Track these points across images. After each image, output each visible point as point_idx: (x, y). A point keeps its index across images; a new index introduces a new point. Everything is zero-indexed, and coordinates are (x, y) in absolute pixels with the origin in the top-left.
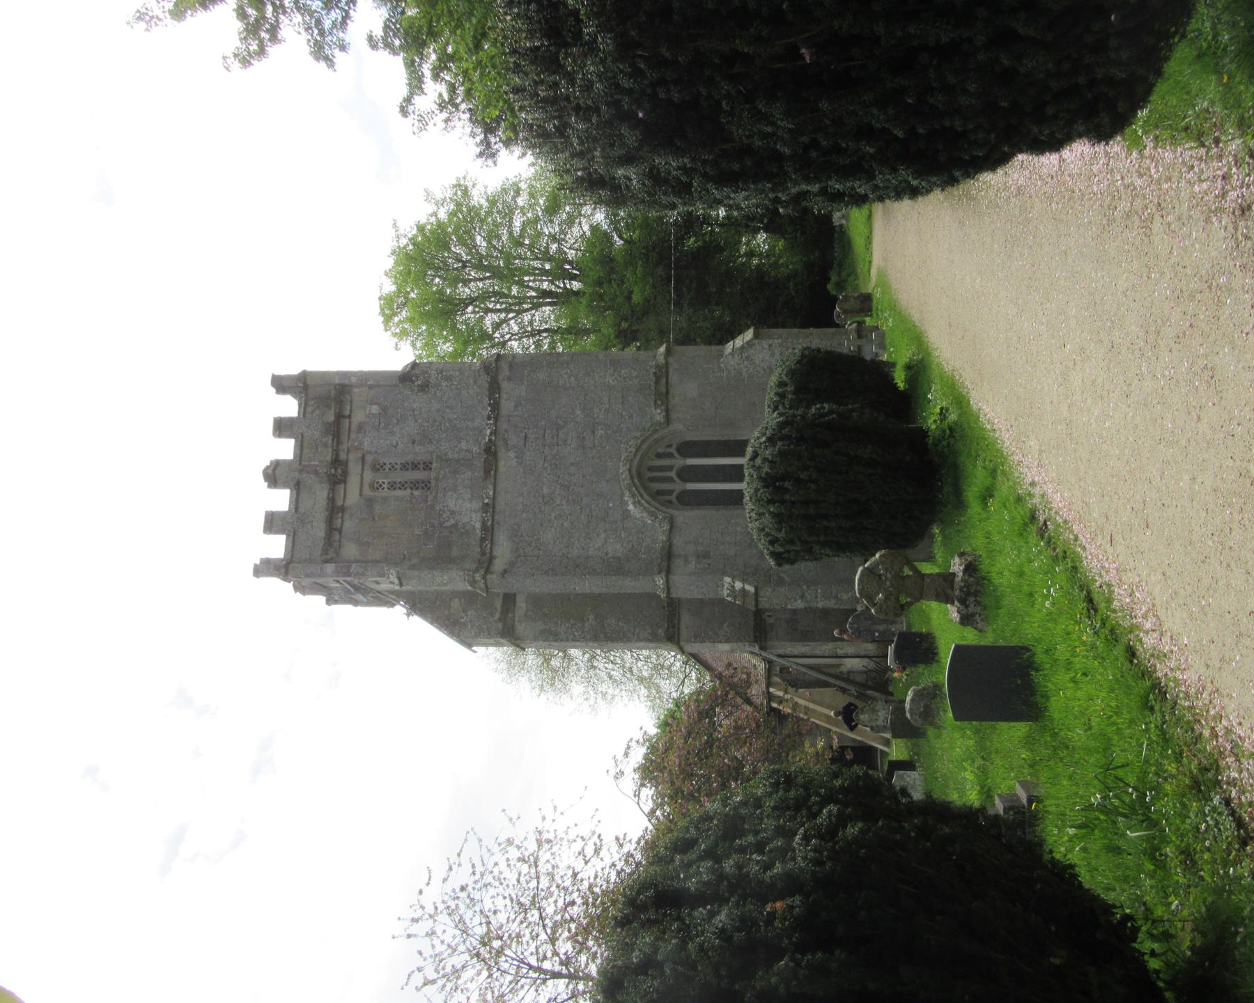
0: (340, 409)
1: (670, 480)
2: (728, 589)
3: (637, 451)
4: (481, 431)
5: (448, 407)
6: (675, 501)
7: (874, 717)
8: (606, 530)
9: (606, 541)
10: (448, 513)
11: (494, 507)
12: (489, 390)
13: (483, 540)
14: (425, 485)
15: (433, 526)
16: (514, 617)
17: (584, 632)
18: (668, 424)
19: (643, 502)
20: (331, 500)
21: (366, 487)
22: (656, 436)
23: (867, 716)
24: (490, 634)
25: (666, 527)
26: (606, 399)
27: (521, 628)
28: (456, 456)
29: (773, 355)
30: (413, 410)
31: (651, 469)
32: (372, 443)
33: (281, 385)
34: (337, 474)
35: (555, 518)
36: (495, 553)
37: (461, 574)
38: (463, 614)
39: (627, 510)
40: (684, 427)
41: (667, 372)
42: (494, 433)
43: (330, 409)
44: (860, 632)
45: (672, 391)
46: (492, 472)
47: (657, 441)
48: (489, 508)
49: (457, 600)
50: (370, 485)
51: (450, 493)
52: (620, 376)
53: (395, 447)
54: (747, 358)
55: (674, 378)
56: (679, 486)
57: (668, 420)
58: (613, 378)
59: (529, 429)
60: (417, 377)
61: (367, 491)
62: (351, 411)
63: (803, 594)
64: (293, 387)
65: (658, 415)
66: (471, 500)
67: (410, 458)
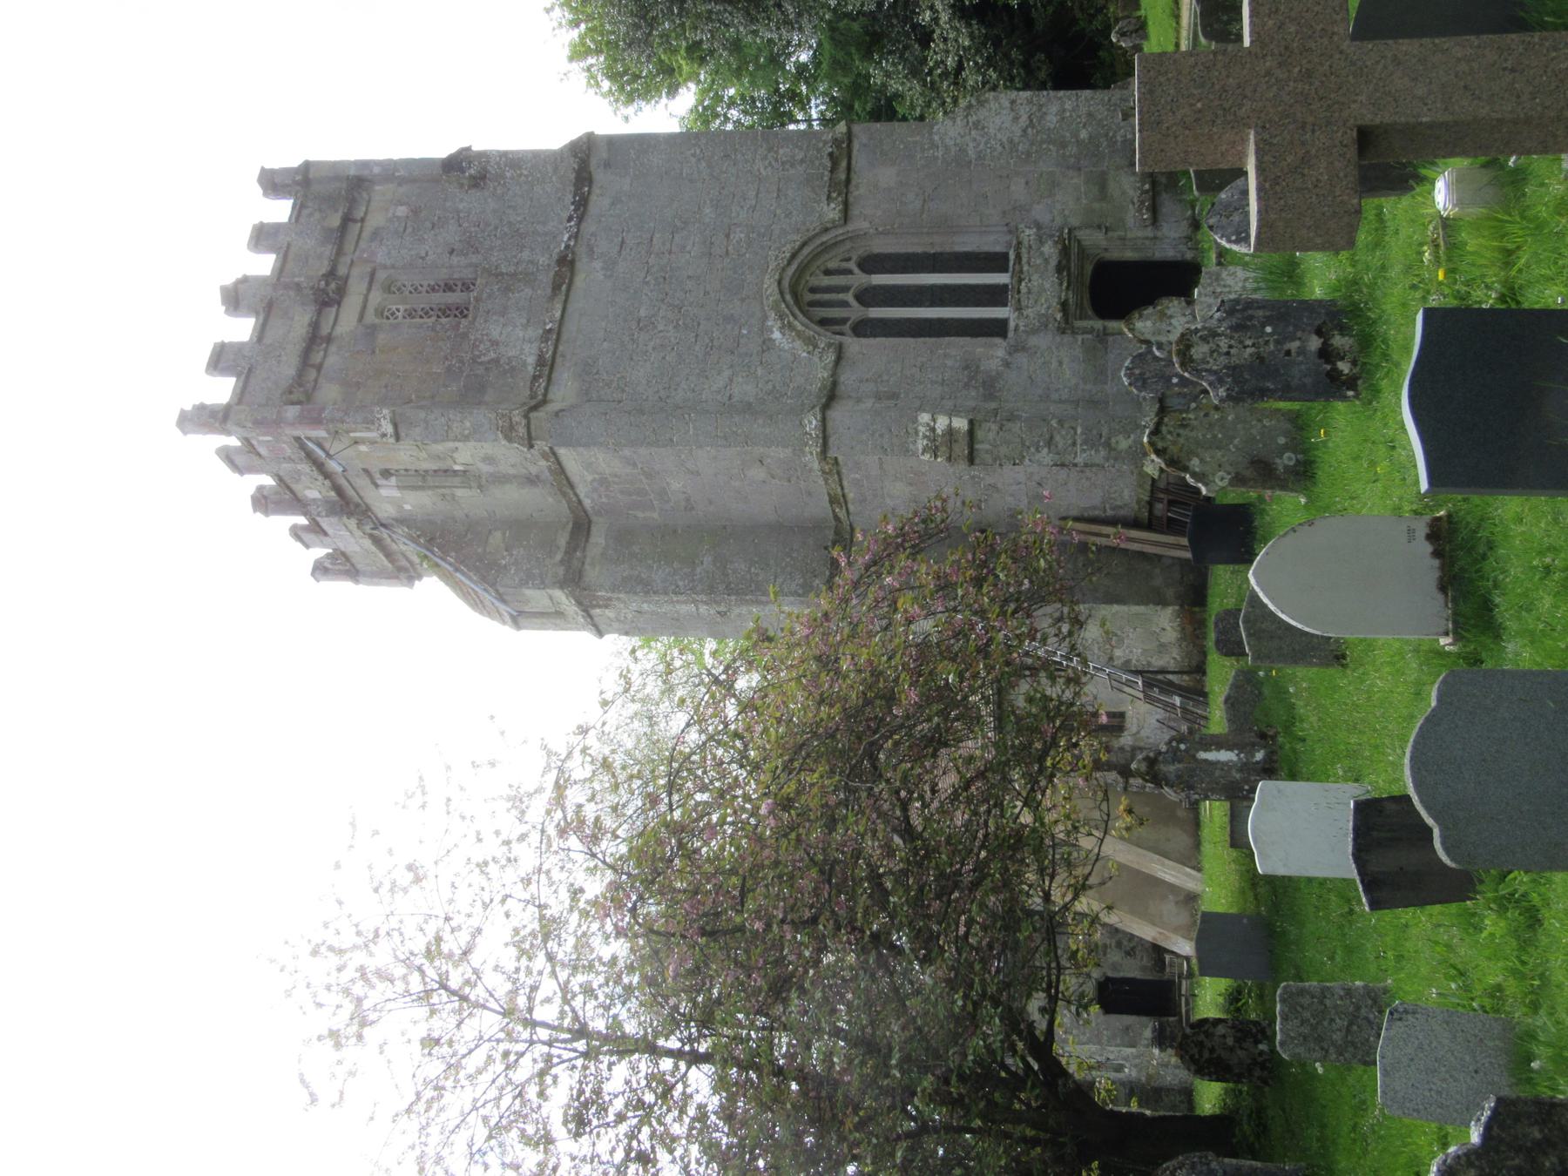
0: (350, 209)
1: (845, 304)
3: (794, 256)
5: (509, 207)
7: (1164, 326)
8: (732, 366)
9: (731, 380)
10: (488, 344)
11: (559, 334)
12: (575, 185)
13: (535, 378)
15: (462, 362)
16: (585, 557)
17: (693, 580)
19: (796, 323)
20: (315, 326)
21: (370, 311)
22: (824, 238)
23: (1149, 323)
24: (543, 583)
25: (830, 357)
26: (752, 194)
27: (592, 574)
28: (512, 269)
29: (1016, 119)
30: (458, 212)
31: (813, 290)
32: (389, 253)
33: (273, 183)
35: (654, 349)
36: (550, 396)
37: (493, 416)
39: (770, 339)
42: (576, 236)
43: (336, 211)
44: (1145, 381)
46: (564, 287)
49: (498, 534)
50: (376, 310)
51: (495, 318)
52: (776, 160)
53: (423, 258)
54: (976, 125)
55: (860, 159)
56: (856, 312)
57: (846, 216)
59: (628, 231)
60: (470, 163)
61: (370, 317)
62: (366, 213)
63: (1052, 438)
64: (288, 186)
65: (832, 212)
66: (525, 327)
67: (443, 274)
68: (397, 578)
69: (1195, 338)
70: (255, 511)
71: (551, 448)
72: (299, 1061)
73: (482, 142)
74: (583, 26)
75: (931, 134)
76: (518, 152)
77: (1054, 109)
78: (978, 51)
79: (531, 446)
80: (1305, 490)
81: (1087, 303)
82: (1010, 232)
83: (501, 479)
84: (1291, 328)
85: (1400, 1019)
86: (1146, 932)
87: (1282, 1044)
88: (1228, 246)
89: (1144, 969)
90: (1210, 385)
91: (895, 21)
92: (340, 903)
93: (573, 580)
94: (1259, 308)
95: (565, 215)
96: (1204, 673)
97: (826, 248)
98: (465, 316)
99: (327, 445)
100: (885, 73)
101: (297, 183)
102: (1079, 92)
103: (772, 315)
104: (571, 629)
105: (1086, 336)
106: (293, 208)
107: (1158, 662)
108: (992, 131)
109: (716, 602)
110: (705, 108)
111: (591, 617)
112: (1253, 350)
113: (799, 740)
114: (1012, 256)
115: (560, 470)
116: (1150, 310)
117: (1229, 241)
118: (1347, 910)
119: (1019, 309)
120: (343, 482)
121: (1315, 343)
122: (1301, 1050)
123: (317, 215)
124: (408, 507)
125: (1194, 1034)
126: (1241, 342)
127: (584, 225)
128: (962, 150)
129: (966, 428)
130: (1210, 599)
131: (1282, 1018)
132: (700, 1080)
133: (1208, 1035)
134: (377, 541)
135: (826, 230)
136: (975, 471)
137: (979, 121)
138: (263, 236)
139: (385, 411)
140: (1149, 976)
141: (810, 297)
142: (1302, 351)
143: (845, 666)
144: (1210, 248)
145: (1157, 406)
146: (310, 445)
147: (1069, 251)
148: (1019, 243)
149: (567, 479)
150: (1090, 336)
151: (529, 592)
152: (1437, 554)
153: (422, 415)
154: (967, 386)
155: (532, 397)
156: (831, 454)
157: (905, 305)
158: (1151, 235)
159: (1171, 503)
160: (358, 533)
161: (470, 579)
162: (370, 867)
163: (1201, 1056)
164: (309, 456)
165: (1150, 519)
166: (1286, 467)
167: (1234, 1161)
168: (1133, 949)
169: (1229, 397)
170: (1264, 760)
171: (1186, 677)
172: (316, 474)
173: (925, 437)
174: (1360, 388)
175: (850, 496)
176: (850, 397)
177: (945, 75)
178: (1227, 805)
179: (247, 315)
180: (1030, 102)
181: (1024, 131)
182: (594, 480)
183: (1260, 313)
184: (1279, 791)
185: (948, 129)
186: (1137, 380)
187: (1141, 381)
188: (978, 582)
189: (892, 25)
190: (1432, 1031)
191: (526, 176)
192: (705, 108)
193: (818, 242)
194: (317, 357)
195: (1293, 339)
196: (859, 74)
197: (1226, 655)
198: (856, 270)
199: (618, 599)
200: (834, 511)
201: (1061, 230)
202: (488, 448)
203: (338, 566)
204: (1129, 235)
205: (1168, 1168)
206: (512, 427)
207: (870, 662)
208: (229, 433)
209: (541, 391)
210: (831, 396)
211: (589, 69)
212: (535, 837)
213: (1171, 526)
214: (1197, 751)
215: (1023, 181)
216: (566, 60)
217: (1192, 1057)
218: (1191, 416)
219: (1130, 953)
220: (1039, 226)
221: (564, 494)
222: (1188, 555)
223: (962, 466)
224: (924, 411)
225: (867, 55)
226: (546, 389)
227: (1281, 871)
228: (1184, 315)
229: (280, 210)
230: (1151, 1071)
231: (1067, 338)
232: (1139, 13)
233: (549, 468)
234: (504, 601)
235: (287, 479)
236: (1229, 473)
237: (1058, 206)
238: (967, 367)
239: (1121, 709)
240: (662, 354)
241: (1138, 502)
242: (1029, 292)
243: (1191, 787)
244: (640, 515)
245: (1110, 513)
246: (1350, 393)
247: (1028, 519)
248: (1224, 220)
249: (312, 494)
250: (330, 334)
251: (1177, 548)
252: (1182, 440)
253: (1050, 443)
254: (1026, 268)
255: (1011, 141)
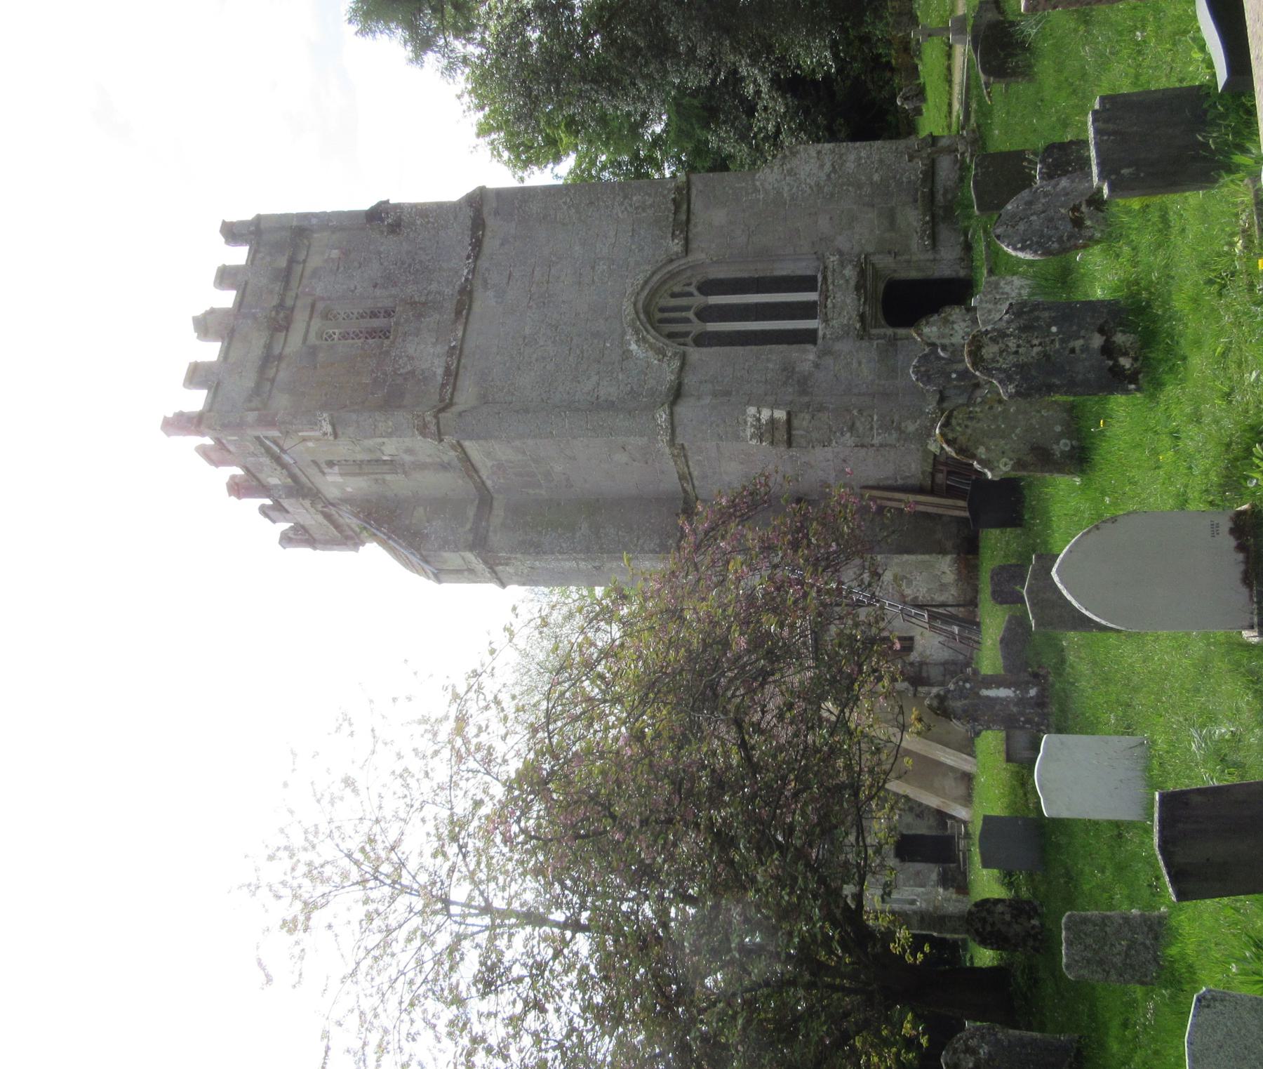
1: (687, 320)
2: (752, 426)
3: (646, 283)
4: (457, 272)
5: (420, 248)
9: (598, 384)
12: (472, 230)
13: (443, 385)
18: (687, 254)
19: (649, 337)
20: (268, 347)
21: (312, 335)
22: (670, 268)
23: (934, 329)
24: (456, 546)
25: (676, 363)
26: (612, 233)
27: (496, 539)
28: (423, 299)
29: (822, 166)
30: (379, 253)
31: (662, 310)
33: (232, 233)
34: (280, 322)
35: (537, 360)
36: (456, 400)
37: (410, 417)
38: (427, 524)
39: (628, 351)
42: (473, 271)
44: (929, 377)
45: (694, 219)
48: (456, 352)
49: (421, 510)
52: (631, 206)
53: (353, 291)
55: (697, 205)
56: (697, 327)
57: (687, 250)
58: (623, 208)
59: (515, 266)
60: (387, 213)
62: (307, 256)
63: (853, 424)
65: (676, 246)
66: (434, 345)
68: (345, 544)
69: (985, 340)
70: (230, 495)
71: (458, 442)
72: (258, 948)
73: (398, 196)
74: (487, 109)
75: (753, 180)
76: (424, 204)
77: (852, 157)
78: (792, 119)
79: (441, 440)
80: (1082, 472)
81: (880, 315)
82: (818, 259)
83: (422, 466)
84: (1075, 328)
85: (1208, 1006)
86: (932, 801)
87: (1068, 967)
88: (1013, 253)
89: (930, 828)
90: (1000, 383)
91: (727, 97)
92: (291, 812)
93: (480, 544)
94: (1044, 309)
95: (465, 254)
96: (976, 606)
97: (672, 276)
98: (388, 338)
99: (281, 442)
100: (720, 139)
101: (251, 233)
102: (872, 143)
103: (630, 331)
104: (480, 582)
105: (879, 341)
106: (249, 253)
107: (940, 598)
108: (803, 177)
109: (592, 559)
110: (583, 172)
111: (496, 573)
112: (1040, 348)
113: (653, 677)
114: (820, 279)
115: (466, 458)
116: (935, 317)
117: (1015, 249)
118: (1116, 833)
119: (826, 321)
120: (296, 471)
121: (1097, 341)
122: (1085, 972)
123: (268, 259)
124: (349, 489)
125: (978, 912)
126: (1029, 342)
127: (479, 262)
128: (779, 193)
129: (785, 418)
130: (981, 550)
131: (1067, 944)
132: (583, 944)
133: (990, 912)
134: (328, 517)
135: (671, 261)
136: (794, 452)
137: (792, 169)
138: (226, 277)
139: (325, 415)
140: (934, 833)
141: (659, 315)
142: (1085, 349)
143: (688, 615)
144: (983, 265)
145: (938, 396)
146: (268, 442)
148: (826, 268)
149: (473, 465)
150: (883, 341)
151: (446, 555)
152: (1241, 548)
153: (354, 416)
154: (785, 383)
155: (442, 400)
156: (679, 440)
157: (734, 320)
158: (932, 257)
159: (949, 473)
160: (312, 510)
161: (400, 545)
162: (312, 783)
163: (984, 929)
164: (268, 451)
165: (932, 486)
166: (1062, 452)
167: (1017, 1032)
168: (922, 812)
169: (1018, 394)
170: (1037, 695)
171: (961, 609)
172: (275, 466)
173: (752, 426)
174: (1141, 382)
175: (695, 474)
176: (692, 395)
177: (766, 138)
178: (1002, 735)
179: (215, 340)
180: (833, 152)
181: (829, 176)
182: (493, 466)
183: (1046, 314)
184: (1062, 743)
185: (769, 176)
186: (922, 376)
187: (925, 377)
188: (795, 546)
189: (725, 101)
190: (1241, 1018)
191: (433, 224)
192: (583, 172)
193: (665, 271)
194: (271, 373)
195: (1078, 338)
196: (699, 141)
197: (1001, 603)
198: (696, 293)
199: (516, 558)
200: (682, 486)
201: (859, 256)
202: (408, 442)
203: (299, 536)
204: (914, 258)
205: (961, 1038)
206: (425, 426)
207: (708, 614)
208: (203, 435)
209: (448, 396)
210: (677, 394)
211: (492, 143)
212: (446, 753)
213: (951, 492)
214: (980, 689)
215: (828, 217)
216: (474, 136)
217: (977, 930)
218: (978, 409)
219: (920, 816)
221: (470, 477)
222: (967, 514)
223: (782, 448)
224: (752, 405)
225: (706, 126)
226: (452, 394)
227: (1065, 814)
228: (964, 321)
229: (239, 255)
230: (937, 903)
231: (865, 344)
232: (918, 82)
233: (458, 456)
234: (427, 562)
235: (252, 470)
236: (1011, 459)
237: (857, 237)
238: (785, 369)
239: (912, 634)
240: (543, 365)
241: (923, 473)
242: (834, 307)
243: (975, 720)
244: (531, 491)
245: (900, 482)
246: (1133, 386)
247: (837, 491)
248: (1010, 230)
249: (274, 481)
250: (281, 354)
251: (957, 509)
252: (969, 431)
253: (852, 428)
254: (831, 287)
255: (818, 185)
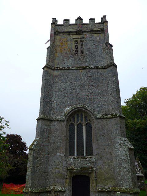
1: (78, 121)
3: (86, 109)
6: (71, 122)
14: (76, 53)
20: (72, 32)
26: (104, 99)
33: (104, 18)
36: (55, 71)
40: (95, 124)
41: (114, 117)
42: (91, 68)
47: (90, 116)
54: (121, 146)
65: (98, 116)
128: (116, 143)
147: (89, 171)
181: (121, 158)
193: (91, 114)
220: (96, 162)
